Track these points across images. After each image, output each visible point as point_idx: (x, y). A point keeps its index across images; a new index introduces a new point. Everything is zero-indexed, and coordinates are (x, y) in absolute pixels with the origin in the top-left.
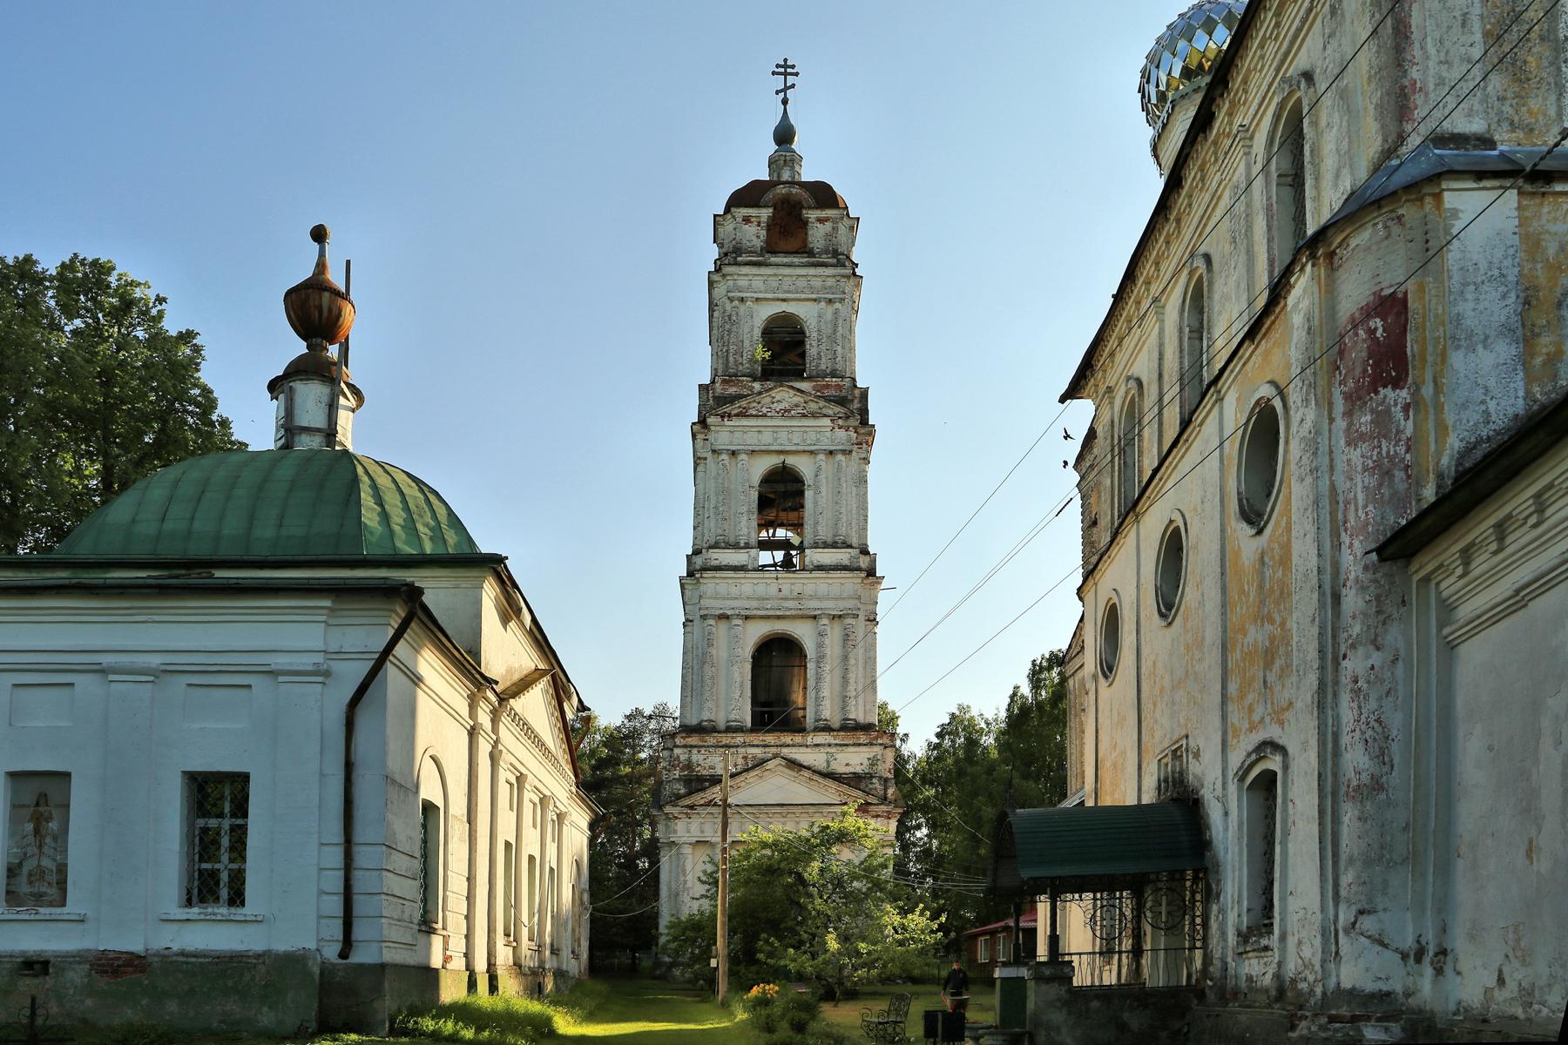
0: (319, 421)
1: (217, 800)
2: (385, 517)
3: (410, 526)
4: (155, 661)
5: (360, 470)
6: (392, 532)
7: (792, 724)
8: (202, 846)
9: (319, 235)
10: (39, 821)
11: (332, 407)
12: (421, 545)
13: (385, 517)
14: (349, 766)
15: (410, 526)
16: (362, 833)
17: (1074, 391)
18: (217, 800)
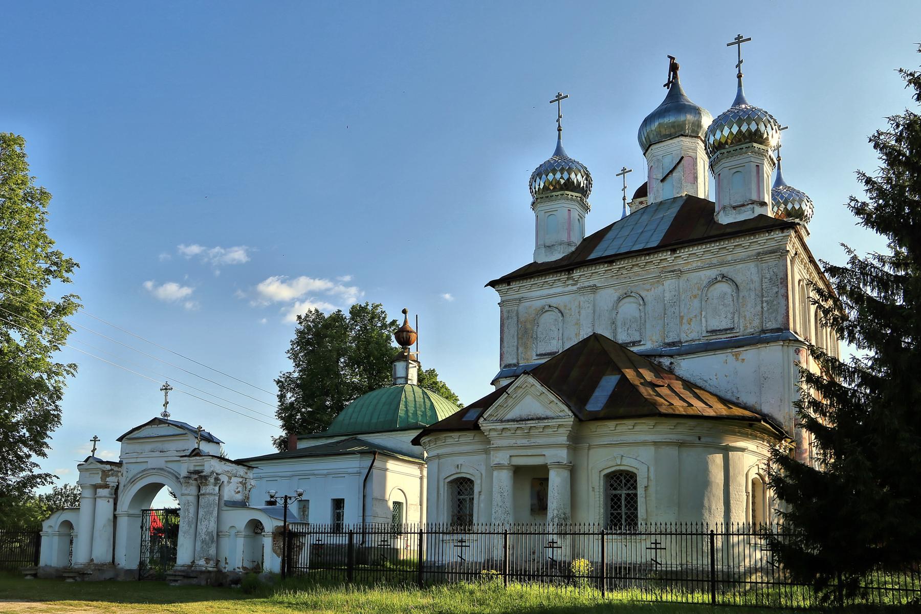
0: (404, 375)
1: (338, 504)
2: (407, 411)
3: (415, 413)
4: (325, 472)
5: (403, 396)
6: (408, 416)
7: (518, 471)
8: (613, 502)
9: (404, 312)
10: (304, 512)
11: (407, 369)
12: (615, 332)
13: (407, 411)
14: (364, 496)
15: (415, 413)
16: (367, 513)
17: (492, 384)
18: (338, 504)
